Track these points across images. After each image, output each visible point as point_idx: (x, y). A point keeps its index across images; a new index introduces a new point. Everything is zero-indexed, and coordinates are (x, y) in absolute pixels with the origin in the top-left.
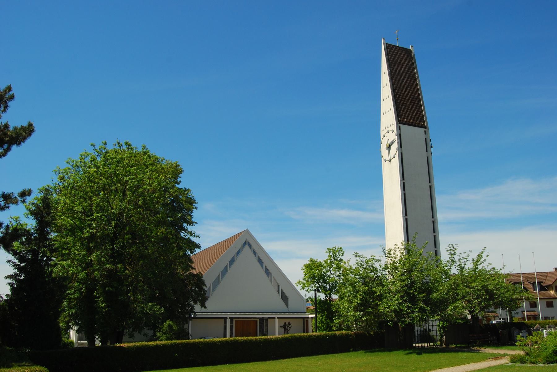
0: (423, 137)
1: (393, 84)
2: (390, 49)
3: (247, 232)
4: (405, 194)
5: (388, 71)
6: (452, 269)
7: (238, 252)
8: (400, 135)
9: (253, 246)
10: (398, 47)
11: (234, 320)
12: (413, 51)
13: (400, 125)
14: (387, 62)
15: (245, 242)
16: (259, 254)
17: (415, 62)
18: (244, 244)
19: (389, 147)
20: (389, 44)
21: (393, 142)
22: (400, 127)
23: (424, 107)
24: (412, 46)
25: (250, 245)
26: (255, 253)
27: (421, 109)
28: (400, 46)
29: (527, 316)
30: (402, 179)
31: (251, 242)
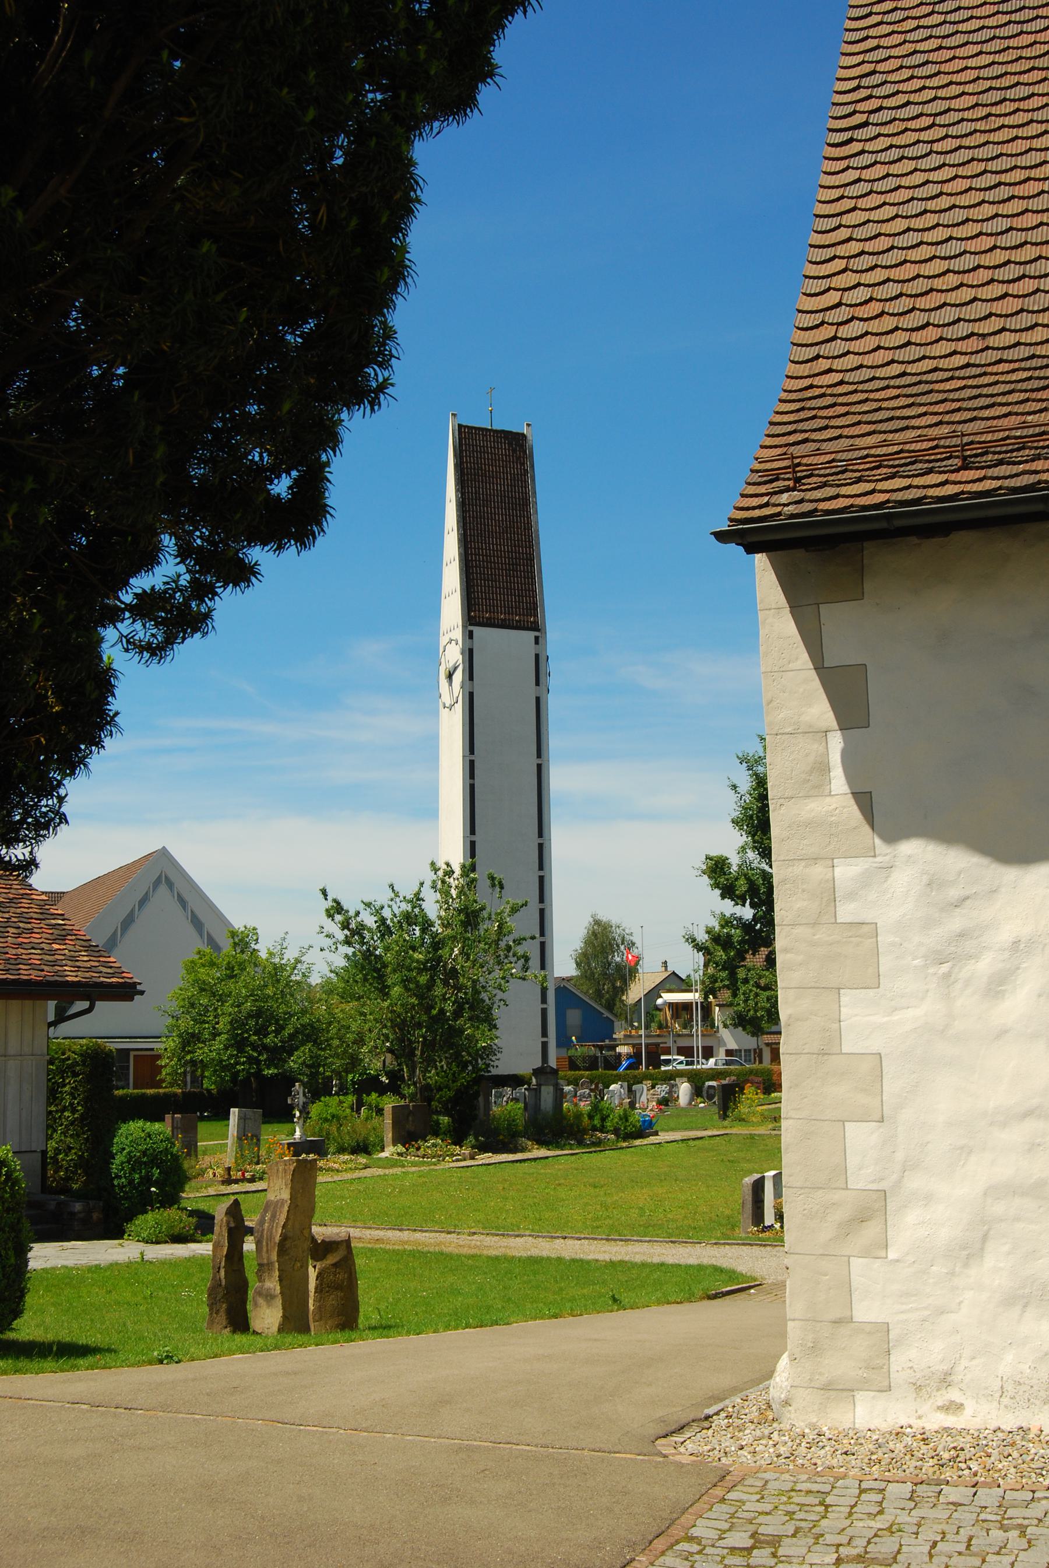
0: (531, 650)
1: (465, 530)
2: (467, 437)
3: (163, 854)
4: (472, 787)
5: (457, 496)
6: (638, 944)
7: (143, 901)
8: (471, 651)
9: (179, 885)
10: (491, 430)
11: (132, 1054)
12: (529, 437)
13: (471, 628)
14: (455, 474)
15: (160, 877)
16: (193, 903)
17: (532, 466)
18: (157, 883)
19: (450, 676)
20: (465, 427)
21: (455, 668)
22: (471, 635)
23: (540, 578)
24: (528, 425)
25: (170, 885)
26: (182, 902)
27: (532, 585)
28: (494, 428)
29: (647, 1045)
30: (468, 753)
31: (173, 878)
